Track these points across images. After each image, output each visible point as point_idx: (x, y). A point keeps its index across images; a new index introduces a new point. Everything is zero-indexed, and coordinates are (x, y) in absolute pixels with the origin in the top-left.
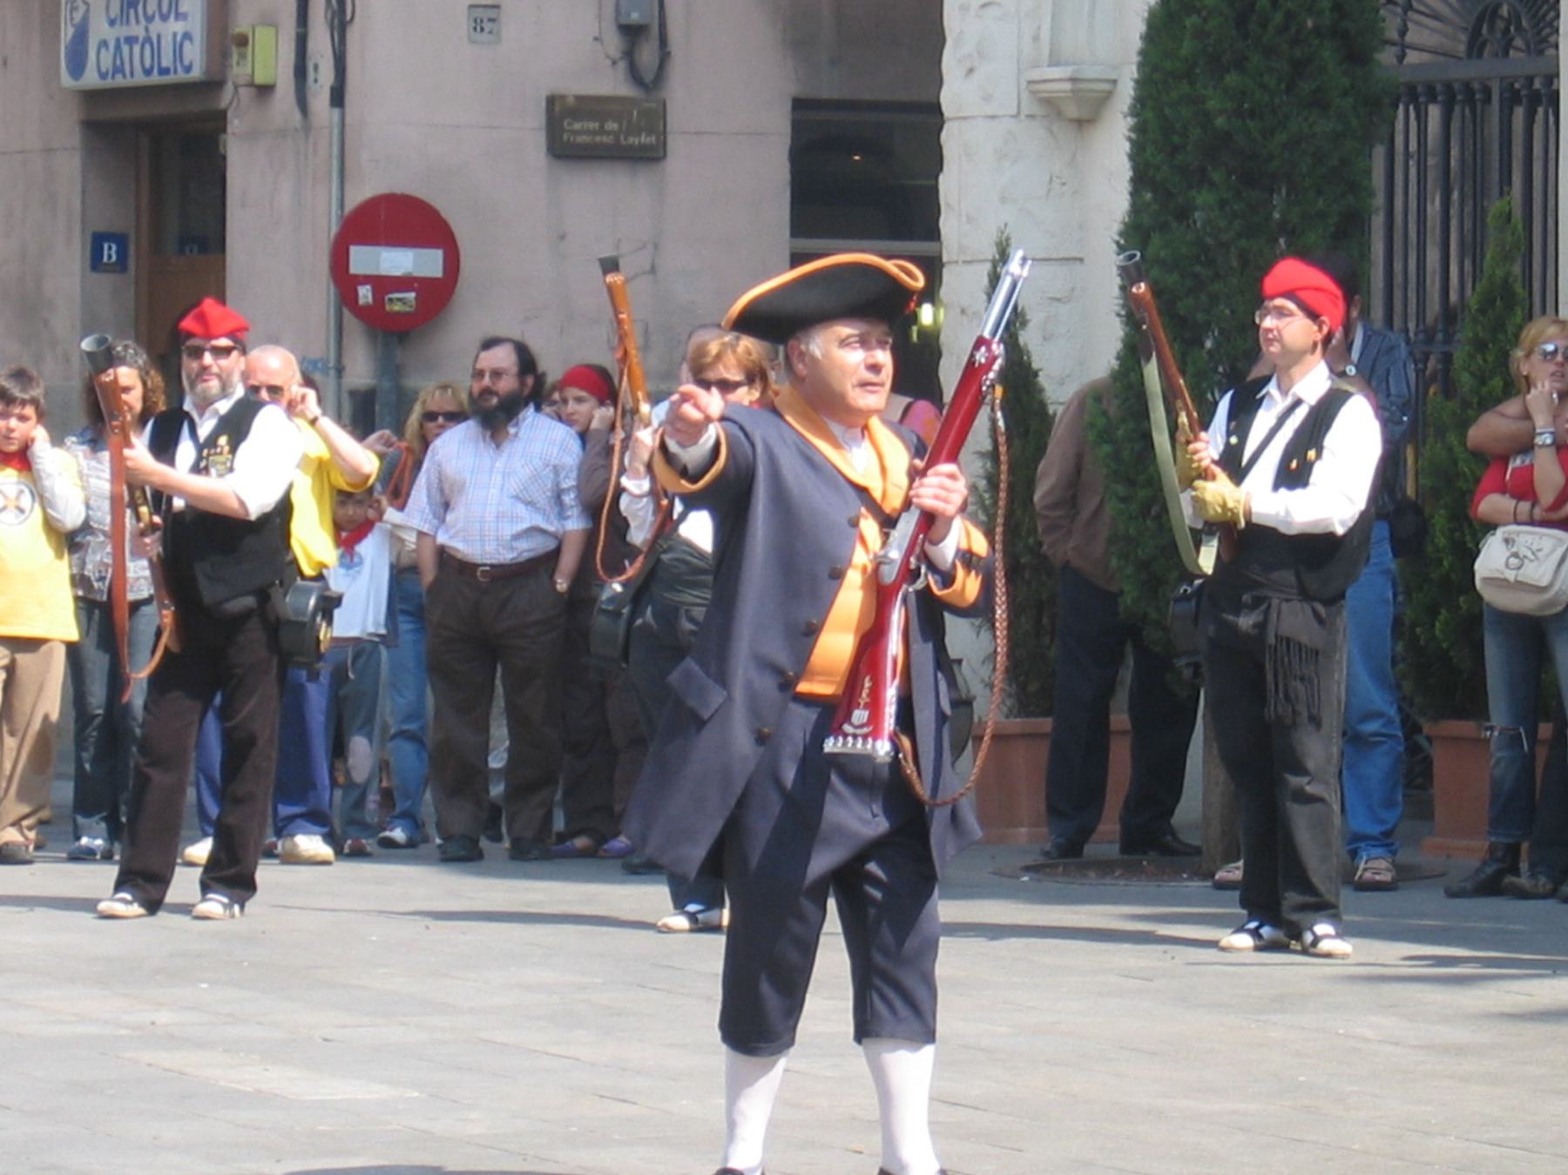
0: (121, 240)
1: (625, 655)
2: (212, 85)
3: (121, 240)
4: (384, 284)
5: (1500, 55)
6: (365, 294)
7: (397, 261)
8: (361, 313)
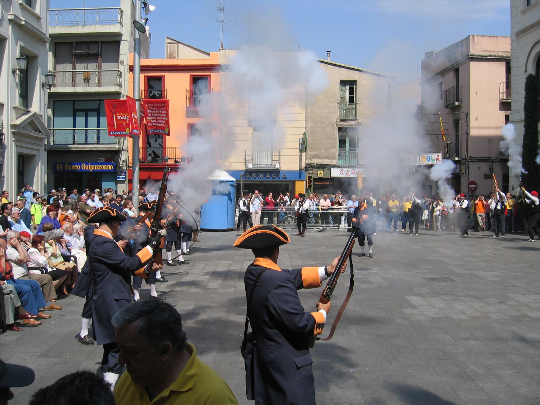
0: (454, 184)
1: (321, 282)
2: (460, 173)
3: (454, 184)
4: (472, 188)
5: (18, 291)
6: (470, 188)
7: (473, 186)
8: (470, 190)
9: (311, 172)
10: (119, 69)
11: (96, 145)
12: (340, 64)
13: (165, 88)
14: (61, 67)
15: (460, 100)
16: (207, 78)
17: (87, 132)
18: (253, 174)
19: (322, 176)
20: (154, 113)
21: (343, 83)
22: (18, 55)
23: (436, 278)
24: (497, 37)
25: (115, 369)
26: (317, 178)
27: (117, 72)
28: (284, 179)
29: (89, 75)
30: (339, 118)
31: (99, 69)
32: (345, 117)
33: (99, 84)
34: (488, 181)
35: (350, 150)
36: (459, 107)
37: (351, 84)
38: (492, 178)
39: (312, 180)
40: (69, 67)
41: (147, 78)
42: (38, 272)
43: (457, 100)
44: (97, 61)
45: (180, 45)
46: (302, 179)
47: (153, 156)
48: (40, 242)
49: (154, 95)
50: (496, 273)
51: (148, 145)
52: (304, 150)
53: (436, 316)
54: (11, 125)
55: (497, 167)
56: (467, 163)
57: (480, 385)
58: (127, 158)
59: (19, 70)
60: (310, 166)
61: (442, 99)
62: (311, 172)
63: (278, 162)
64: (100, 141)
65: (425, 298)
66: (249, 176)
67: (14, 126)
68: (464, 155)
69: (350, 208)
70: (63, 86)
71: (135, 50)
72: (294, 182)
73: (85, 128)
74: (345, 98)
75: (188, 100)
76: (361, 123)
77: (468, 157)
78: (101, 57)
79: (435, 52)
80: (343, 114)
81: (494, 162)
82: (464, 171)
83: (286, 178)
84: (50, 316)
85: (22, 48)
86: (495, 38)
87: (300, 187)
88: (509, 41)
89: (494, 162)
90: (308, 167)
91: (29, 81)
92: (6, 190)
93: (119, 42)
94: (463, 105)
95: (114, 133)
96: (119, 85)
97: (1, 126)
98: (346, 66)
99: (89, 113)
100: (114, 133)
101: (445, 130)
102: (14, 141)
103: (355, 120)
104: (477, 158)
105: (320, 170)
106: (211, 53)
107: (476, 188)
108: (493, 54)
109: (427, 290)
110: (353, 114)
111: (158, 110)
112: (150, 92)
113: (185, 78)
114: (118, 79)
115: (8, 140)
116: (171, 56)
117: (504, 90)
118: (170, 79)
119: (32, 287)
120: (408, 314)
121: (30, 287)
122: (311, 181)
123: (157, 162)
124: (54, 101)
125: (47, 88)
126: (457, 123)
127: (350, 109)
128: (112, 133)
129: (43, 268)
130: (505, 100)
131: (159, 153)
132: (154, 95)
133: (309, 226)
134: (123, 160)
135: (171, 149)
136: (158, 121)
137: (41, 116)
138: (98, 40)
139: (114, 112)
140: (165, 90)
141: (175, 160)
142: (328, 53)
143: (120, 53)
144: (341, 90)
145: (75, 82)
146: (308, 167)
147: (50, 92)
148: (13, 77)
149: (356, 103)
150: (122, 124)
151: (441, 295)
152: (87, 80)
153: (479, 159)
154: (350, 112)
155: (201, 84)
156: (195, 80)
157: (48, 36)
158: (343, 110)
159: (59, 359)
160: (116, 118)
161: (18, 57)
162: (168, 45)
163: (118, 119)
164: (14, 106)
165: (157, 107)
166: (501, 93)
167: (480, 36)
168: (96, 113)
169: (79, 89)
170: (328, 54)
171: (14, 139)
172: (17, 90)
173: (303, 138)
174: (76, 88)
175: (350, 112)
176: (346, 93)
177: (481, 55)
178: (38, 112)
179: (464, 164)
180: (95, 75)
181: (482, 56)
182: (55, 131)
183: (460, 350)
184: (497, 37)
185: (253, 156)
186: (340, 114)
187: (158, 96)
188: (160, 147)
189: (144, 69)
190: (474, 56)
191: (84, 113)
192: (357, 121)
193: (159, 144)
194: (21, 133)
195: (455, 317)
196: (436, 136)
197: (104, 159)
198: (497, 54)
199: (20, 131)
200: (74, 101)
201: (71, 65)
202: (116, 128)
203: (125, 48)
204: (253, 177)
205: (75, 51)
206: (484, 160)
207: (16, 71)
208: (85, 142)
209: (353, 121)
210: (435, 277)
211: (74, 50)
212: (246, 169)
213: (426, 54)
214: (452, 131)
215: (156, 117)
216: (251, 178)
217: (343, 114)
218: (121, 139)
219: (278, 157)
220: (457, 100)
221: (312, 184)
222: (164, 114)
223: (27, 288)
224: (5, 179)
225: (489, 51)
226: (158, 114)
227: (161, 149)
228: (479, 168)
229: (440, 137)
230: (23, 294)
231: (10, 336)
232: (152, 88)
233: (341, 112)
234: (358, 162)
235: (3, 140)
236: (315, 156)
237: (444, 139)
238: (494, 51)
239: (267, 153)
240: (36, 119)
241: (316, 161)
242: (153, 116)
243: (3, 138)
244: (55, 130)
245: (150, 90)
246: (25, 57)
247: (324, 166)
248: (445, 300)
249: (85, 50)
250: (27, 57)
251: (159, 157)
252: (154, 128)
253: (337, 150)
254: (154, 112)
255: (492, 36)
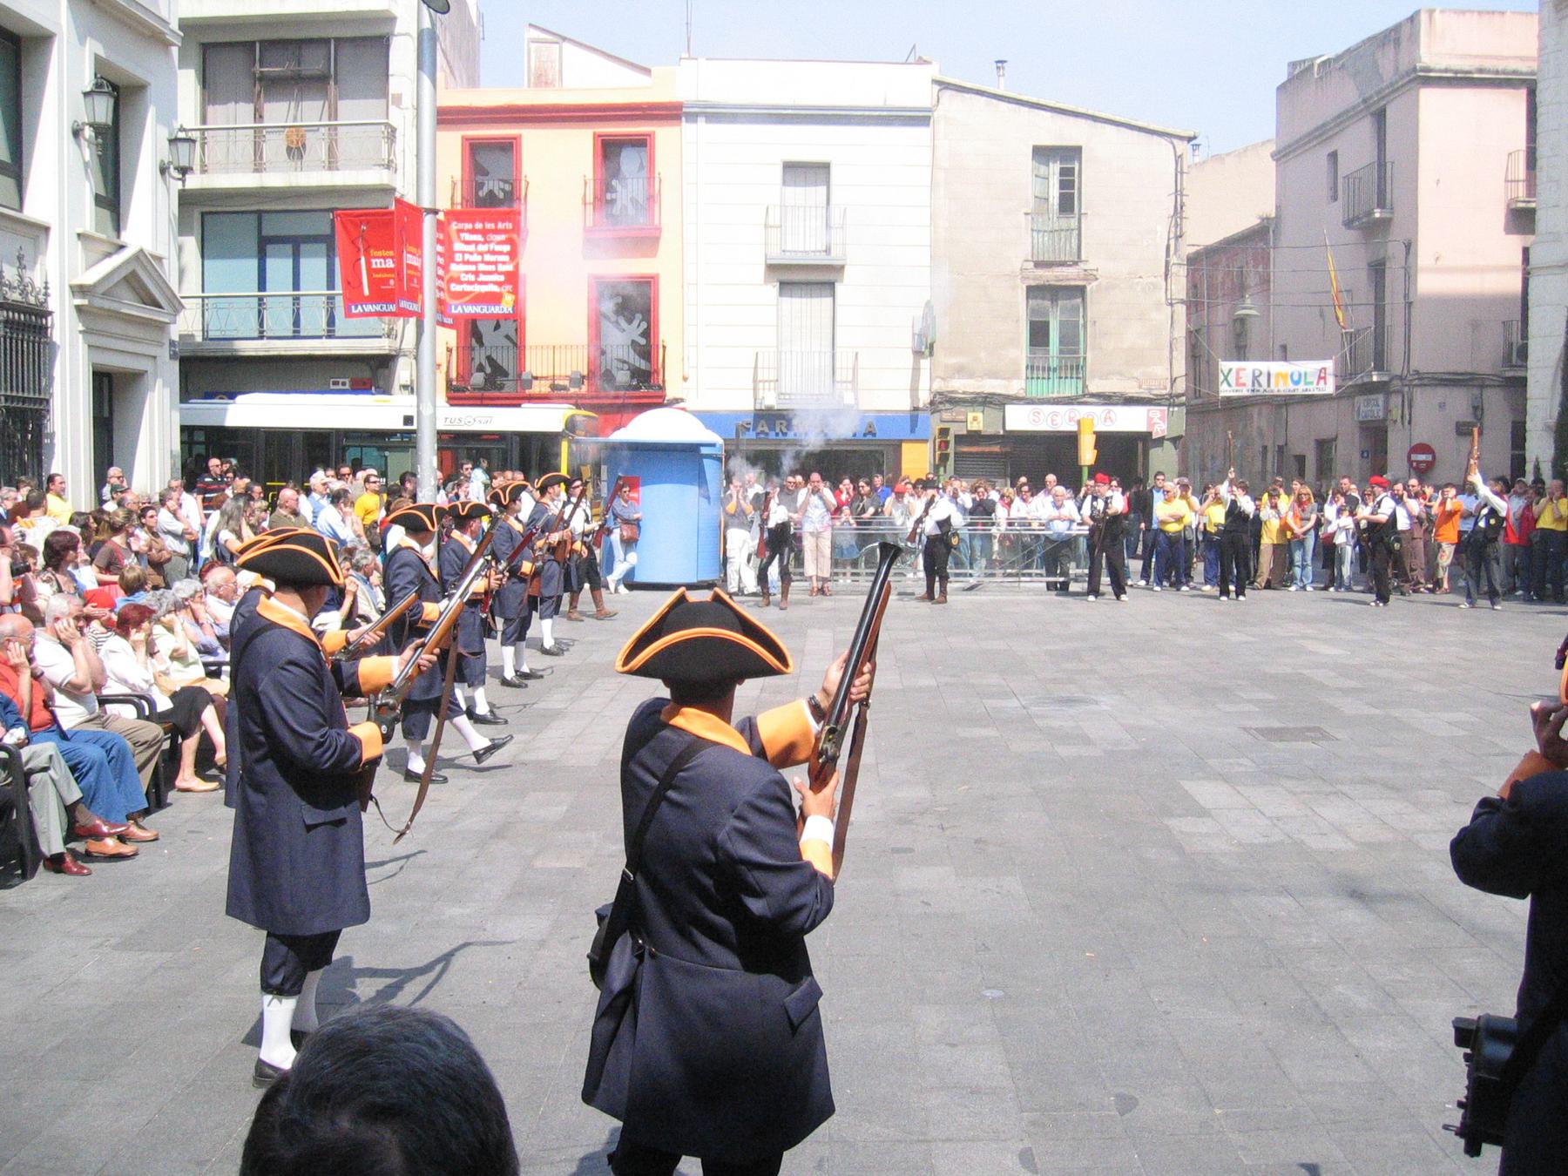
2: (1385, 420)
3: (1368, 452)
4: (1419, 462)
5: (70, 763)
6: (1415, 464)
7: (1422, 457)
8: (1415, 469)
9: (946, 416)
10: (387, 118)
11: (324, 340)
12: (1034, 100)
13: (520, 172)
14: (221, 114)
15: (1388, 206)
16: (641, 143)
17: (298, 304)
18: (778, 422)
19: (981, 428)
20: (471, 253)
21: (1043, 154)
22: (88, 82)
23: (1283, 729)
24: (1503, 13)
25: (287, 986)
26: (965, 433)
27: (383, 128)
28: (869, 437)
29: (302, 136)
30: (1030, 258)
31: (330, 120)
32: (1046, 255)
33: (332, 164)
34: (1464, 443)
35: (1061, 352)
36: (1385, 224)
37: (1066, 157)
38: (1471, 434)
39: (951, 438)
40: (242, 112)
41: (471, 144)
42: (129, 712)
43: (1381, 204)
44: (324, 94)
45: (566, 45)
46: (919, 434)
47: (488, 370)
48: (138, 625)
49: (491, 192)
50: (1460, 716)
51: (474, 340)
52: (927, 352)
53: (1263, 840)
54: (71, 287)
55: (1495, 402)
56: (1406, 389)
57: (1355, 1041)
58: (414, 378)
59: (91, 125)
60: (946, 400)
61: (1335, 198)
62: (946, 416)
63: (850, 386)
64: (336, 328)
65: (1238, 788)
66: (766, 430)
67: (80, 290)
68: (1397, 367)
69: (1052, 520)
70: (227, 171)
71: (420, 67)
72: (896, 446)
73: (294, 290)
74: (1047, 200)
75: (590, 208)
76: (1095, 273)
77: (1408, 371)
78: (336, 83)
79: (1319, 61)
80: (1041, 246)
81: (1487, 386)
82: (1396, 414)
83: (874, 435)
84: (157, 835)
85: (98, 60)
86: (1497, 18)
87: (916, 460)
88: (1533, 25)
89: (1487, 386)
90: (941, 403)
91: (121, 153)
92: (60, 473)
93: (388, 40)
94: (1398, 218)
95: (360, 307)
96: (389, 165)
97: (43, 291)
98: (1052, 103)
99: (304, 247)
100: (360, 307)
101: (1345, 294)
102: (80, 332)
103: (1076, 263)
104: (1440, 376)
105: (974, 411)
106: (653, 69)
107: (1430, 465)
108: (1488, 64)
109: (1250, 763)
110: (1071, 247)
111: (485, 242)
112: (480, 186)
113: (579, 143)
114: (385, 147)
115: (64, 328)
116: (541, 80)
117: (1521, 172)
118: (535, 143)
119: (108, 752)
120: (1182, 832)
121: (104, 753)
122: (947, 444)
123: (501, 387)
124: (203, 214)
125: (174, 178)
126: (1378, 270)
127: (1062, 230)
128: (356, 308)
129: (141, 697)
130: (1524, 202)
131: (505, 360)
132: (491, 192)
133: (957, 575)
134: (403, 383)
135: (563, 351)
136: (482, 278)
137: (159, 259)
138: (323, 34)
139: (361, 246)
140: (523, 178)
141: (550, 382)
142: (1000, 65)
143: (391, 72)
144: (1036, 176)
145: (261, 158)
146: (941, 403)
147: (184, 190)
148: (76, 147)
149: (1080, 215)
150: (386, 281)
151: (1287, 777)
152: (296, 151)
153: (1442, 380)
154: (1063, 240)
155: (629, 160)
156: (609, 150)
157: (175, 26)
158: (1041, 235)
159: (171, 954)
160: (368, 264)
161: (88, 89)
162: (533, 46)
163: (374, 266)
164: (80, 230)
165: (484, 232)
166: (1512, 181)
167: (1450, 10)
168: (323, 247)
169: (276, 178)
170: (998, 68)
171: (81, 328)
172: (87, 184)
173: (924, 317)
174: (264, 174)
175: (1063, 240)
176: (1051, 184)
177: (1453, 68)
178: (149, 248)
179: (1395, 392)
180: (320, 136)
181: (1456, 72)
182: (206, 301)
183: (1315, 941)
184: (1503, 13)
185: (778, 369)
186: (1033, 247)
187: (501, 195)
188: (511, 345)
189: (448, 117)
190: (1430, 70)
191: (289, 248)
192: (1082, 266)
193: (507, 337)
194: (101, 309)
195: (1314, 843)
196: (1317, 310)
197: (347, 381)
198: (1501, 65)
199: (98, 302)
200: (260, 213)
201: (250, 107)
202: (366, 292)
203: (402, 54)
204: (778, 430)
205: (261, 67)
206: (1463, 380)
207: (82, 130)
208: (294, 332)
209: (1070, 266)
210: (1276, 724)
211: (257, 65)
212: (758, 407)
213: (1293, 65)
214: (1365, 294)
215: (476, 263)
216: (772, 435)
217: (1041, 246)
218: (395, 323)
219: (851, 372)
220: (1381, 204)
221: (951, 450)
222: (501, 253)
223: (94, 753)
224: (58, 440)
225: (1476, 57)
226: (481, 254)
227: (511, 352)
228: (1442, 406)
229: (1329, 312)
230: (84, 770)
231: (42, 887)
232: (486, 174)
233: (1036, 241)
234: (1085, 386)
235: (49, 330)
236: (960, 371)
237: (1341, 320)
238: (1496, 58)
239: (820, 366)
240: (145, 268)
241: (963, 386)
242: (468, 263)
243: (49, 324)
244: (208, 297)
245: (480, 178)
246: (106, 90)
247: (986, 397)
248: (1295, 794)
249: (290, 65)
250: (115, 87)
251: (506, 374)
252: (467, 298)
253: (1024, 351)
254: (471, 248)
255: (1488, 13)
